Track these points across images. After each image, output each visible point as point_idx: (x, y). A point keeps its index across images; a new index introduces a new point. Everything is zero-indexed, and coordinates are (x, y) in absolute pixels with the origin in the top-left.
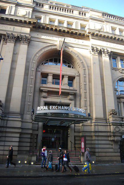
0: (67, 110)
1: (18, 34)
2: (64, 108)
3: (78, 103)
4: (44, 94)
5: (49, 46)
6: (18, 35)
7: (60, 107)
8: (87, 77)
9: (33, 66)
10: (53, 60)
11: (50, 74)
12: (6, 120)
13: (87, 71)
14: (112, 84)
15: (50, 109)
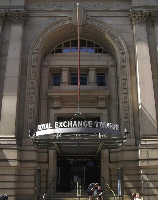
0: (83, 126)
1: (5, 11)
2: (77, 125)
3: (114, 112)
4: (56, 103)
5: (58, 22)
6: (7, 12)
7: (70, 123)
8: (127, 67)
9: (34, 58)
10: (71, 43)
11: (64, 68)
12: (59, 147)
13: (127, 55)
14: (16, 109)
15: (56, 127)
